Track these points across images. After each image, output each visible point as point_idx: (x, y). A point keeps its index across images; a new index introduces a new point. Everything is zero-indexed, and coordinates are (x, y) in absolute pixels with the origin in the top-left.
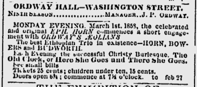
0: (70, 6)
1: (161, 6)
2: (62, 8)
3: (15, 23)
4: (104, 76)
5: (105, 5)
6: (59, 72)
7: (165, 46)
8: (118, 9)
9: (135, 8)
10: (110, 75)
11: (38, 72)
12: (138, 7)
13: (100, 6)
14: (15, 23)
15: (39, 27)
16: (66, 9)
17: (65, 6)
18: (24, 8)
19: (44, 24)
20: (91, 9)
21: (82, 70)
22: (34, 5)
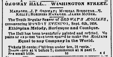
0: (37, 3)
1: (95, 3)
3: (11, 10)
5: (62, 3)
6: (43, 29)
8: (70, 5)
9: (79, 4)
10: (51, 49)
11: (23, 48)
12: (81, 4)
16: (23, 5)
18: (96, 5)
19: (10, 12)
20: (19, 5)
21: (47, 46)
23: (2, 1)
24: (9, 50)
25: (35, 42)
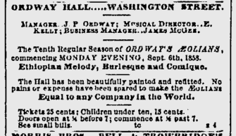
0: (79, 6)
4: (161, 117)
5: (130, 5)
7: (143, 60)
11: (48, 114)
13: (124, 6)
14: (23, 22)
16: (75, 9)
17: (74, 6)
22: (35, 5)
24: (20, 117)
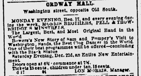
2: (119, 38)
15: (30, 22)
23: (5, 75)
25: (27, 64)
